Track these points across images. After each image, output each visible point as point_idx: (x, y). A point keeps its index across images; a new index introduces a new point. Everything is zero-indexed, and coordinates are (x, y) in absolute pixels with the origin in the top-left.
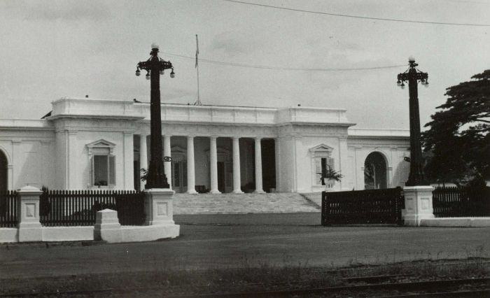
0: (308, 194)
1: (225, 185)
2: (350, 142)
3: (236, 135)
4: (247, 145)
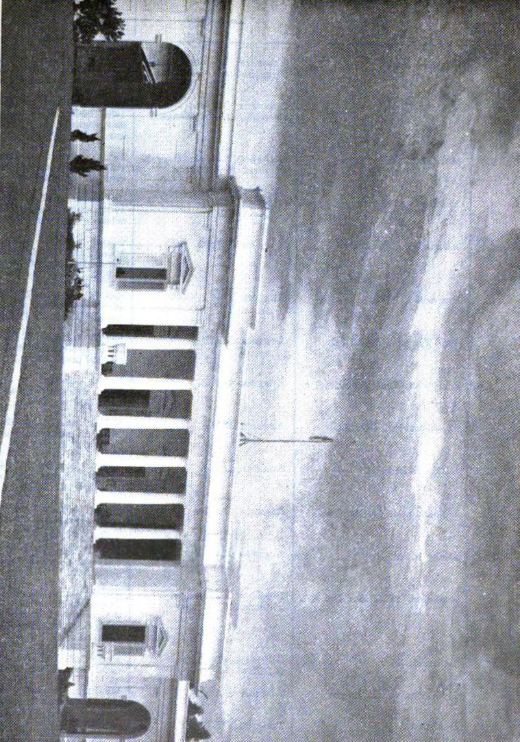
0: (89, 616)
1: (108, 478)
2: (168, 684)
3: (196, 386)
4: (172, 516)
